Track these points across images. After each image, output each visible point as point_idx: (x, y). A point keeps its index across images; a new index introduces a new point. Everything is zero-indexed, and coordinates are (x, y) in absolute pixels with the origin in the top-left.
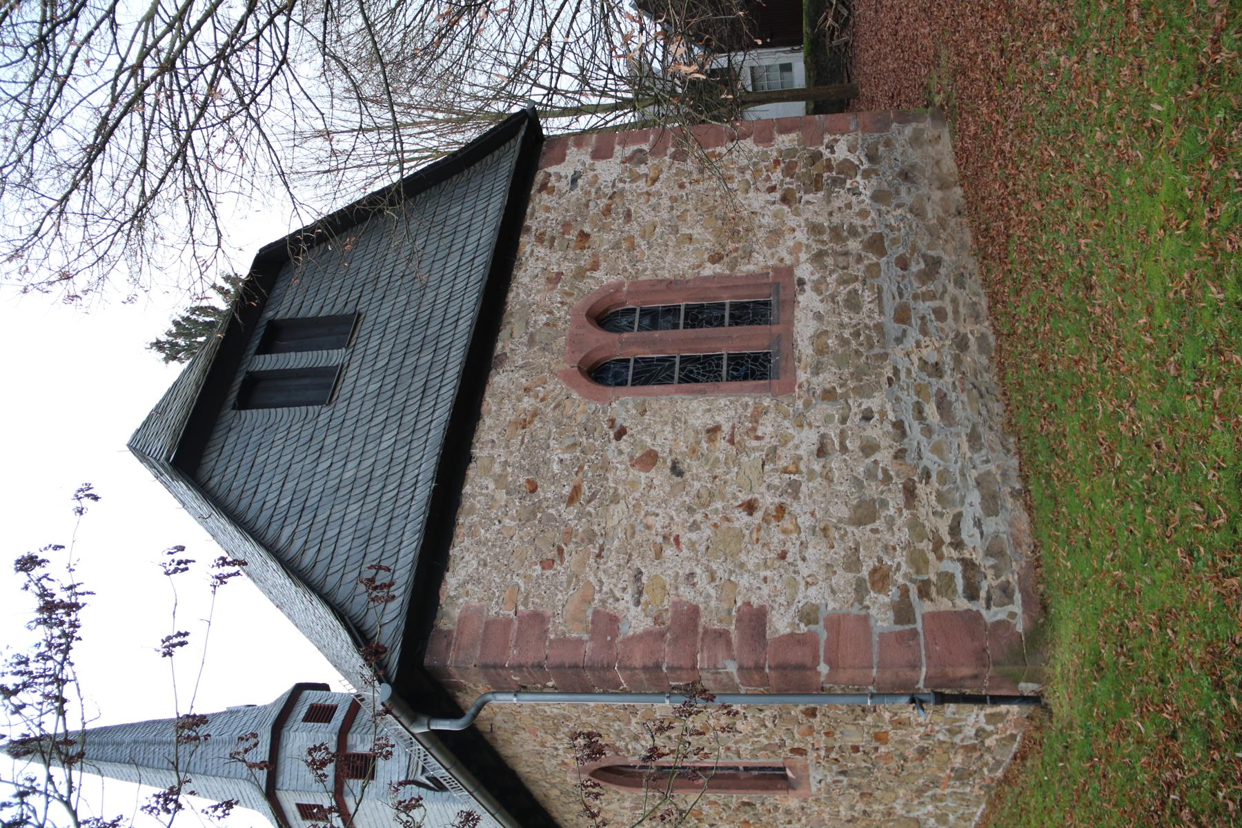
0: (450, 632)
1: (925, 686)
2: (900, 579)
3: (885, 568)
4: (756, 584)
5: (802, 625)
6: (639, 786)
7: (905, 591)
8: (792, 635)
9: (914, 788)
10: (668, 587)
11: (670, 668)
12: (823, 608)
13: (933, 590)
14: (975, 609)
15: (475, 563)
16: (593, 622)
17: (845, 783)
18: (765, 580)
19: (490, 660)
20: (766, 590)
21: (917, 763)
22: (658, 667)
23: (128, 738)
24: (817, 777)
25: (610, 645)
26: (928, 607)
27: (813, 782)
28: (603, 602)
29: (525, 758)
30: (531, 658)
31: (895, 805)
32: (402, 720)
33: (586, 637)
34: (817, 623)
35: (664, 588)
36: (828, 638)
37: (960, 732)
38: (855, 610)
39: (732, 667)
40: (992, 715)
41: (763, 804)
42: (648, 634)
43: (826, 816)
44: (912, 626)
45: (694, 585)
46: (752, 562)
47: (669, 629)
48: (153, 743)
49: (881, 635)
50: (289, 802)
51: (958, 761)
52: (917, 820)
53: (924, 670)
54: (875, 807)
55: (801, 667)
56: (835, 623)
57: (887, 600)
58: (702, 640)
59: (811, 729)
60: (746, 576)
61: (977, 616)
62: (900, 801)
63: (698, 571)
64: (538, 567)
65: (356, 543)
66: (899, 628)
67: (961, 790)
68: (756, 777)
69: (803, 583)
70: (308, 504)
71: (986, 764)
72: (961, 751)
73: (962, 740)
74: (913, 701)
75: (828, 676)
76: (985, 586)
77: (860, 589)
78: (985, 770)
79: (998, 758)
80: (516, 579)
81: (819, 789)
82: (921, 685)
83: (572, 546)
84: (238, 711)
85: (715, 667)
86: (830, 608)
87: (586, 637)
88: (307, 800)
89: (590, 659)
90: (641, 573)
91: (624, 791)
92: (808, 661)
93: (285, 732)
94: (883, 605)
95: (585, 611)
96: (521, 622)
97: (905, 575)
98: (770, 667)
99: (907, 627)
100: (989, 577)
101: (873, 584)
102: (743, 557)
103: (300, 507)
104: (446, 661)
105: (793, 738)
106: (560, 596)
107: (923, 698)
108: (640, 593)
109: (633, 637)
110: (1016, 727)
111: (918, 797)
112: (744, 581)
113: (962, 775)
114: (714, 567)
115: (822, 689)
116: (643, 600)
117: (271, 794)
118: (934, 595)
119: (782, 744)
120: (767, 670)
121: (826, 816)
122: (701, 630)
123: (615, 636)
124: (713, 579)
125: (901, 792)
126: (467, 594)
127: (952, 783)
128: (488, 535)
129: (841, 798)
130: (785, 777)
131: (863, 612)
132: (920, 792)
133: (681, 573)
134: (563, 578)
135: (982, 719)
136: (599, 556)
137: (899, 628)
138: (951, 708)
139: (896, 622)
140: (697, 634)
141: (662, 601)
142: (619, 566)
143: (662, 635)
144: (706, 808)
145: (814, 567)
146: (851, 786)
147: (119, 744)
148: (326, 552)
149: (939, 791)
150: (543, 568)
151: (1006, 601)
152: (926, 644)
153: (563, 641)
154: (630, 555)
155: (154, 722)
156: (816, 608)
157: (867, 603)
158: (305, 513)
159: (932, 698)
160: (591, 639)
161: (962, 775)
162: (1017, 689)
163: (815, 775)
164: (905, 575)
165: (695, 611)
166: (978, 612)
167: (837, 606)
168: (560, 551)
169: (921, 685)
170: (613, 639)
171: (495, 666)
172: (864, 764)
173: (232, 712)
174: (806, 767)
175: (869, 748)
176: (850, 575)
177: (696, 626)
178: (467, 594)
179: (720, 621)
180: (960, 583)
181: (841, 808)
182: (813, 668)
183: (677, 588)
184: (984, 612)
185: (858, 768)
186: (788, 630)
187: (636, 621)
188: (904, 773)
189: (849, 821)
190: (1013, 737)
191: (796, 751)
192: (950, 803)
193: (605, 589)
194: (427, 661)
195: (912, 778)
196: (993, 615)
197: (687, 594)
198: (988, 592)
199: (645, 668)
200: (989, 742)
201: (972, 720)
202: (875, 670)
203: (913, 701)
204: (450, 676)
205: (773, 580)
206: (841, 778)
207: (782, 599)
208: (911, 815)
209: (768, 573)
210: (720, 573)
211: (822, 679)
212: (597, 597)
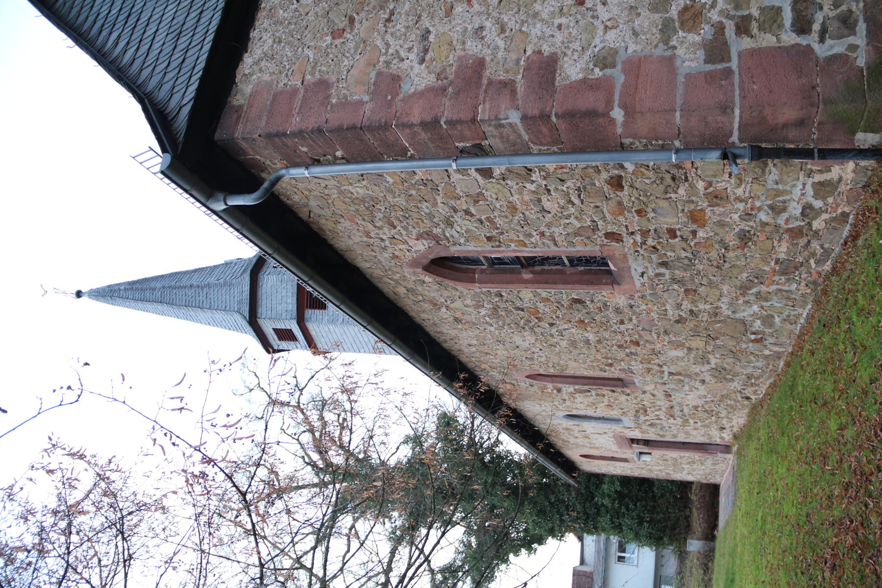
0: (240, 107)
1: (741, 140)
2: (714, 16)
3: (698, 6)
4: (548, 32)
5: (597, 70)
6: (472, 281)
7: (720, 29)
8: (584, 81)
9: (738, 284)
10: (455, 42)
11: (449, 122)
12: (622, 52)
13: (754, 25)
14: (804, 43)
15: (270, 41)
16: (374, 84)
17: (667, 277)
18: (560, 27)
19: (273, 130)
20: (559, 37)
21: (739, 252)
22: (436, 121)
23: (158, 285)
24: (638, 268)
25: (390, 104)
26: (746, 43)
27: (636, 275)
28: (388, 63)
29: (359, 252)
30: (311, 123)
31: (720, 304)
32: (194, 193)
33: (366, 98)
34: (614, 67)
35: (450, 44)
36: (626, 80)
37: (784, 210)
38: (660, 51)
39: (514, 117)
40: (821, 184)
41: (592, 301)
42: (430, 90)
43: (655, 316)
44: (725, 65)
45: (482, 38)
46: (546, 11)
47: (451, 83)
48: (174, 288)
49: (688, 76)
50: (268, 328)
51: (783, 250)
52: (743, 322)
53: (737, 112)
54: (702, 306)
55: (591, 114)
56: (635, 67)
57: (697, 38)
58: (486, 92)
59: (621, 208)
60: (539, 25)
61: (809, 49)
62: (725, 300)
63: (488, 24)
64: (329, 39)
65: (170, 37)
66: (709, 67)
67: (786, 288)
68: (581, 273)
69: (602, 27)
70: (134, 10)
71: (813, 254)
72: (786, 236)
73: (787, 221)
74: (725, 156)
75: (625, 124)
76: (819, 17)
77: (667, 30)
78: (812, 261)
79: (826, 246)
80: (306, 51)
81: (643, 284)
82: (735, 138)
83: (363, 14)
84: (231, 263)
85: (497, 118)
86: (630, 51)
87: (366, 98)
88: (280, 326)
89: (368, 119)
90: (429, 32)
91: (461, 287)
92: (601, 107)
93: (261, 276)
94: (693, 44)
95: (369, 73)
96: (306, 90)
97: (721, 12)
98: (556, 115)
99: (719, 66)
100: (825, 8)
101: (682, 24)
102: (538, 7)
103: (127, 14)
104: (234, 134)
105: (604, 218)
106: (346, 63)
107: (737, 151)
108: (426, 51)
109: (414, 94)
110: (849, 203)
111: (743, 295)
112: (537, 30)
113: (787, 269)
114: (506, 20)
115: (622, 145)
116: (428, 57)
117: (253, 322)
118: (755, 31)
119: (595, 229)
120: (554, 119)
121: (655, 316)
122: (485, 82)
123: (395, 95)
124: (503, 31)
125: (725, 288)
126: (261, 70)
127: (776, 278)
128: (286, 15)
129: (666, 295)
130: (610, 272)
131: (669, 53)
132: (744, 289)
133: (470, 27)
134: (351, 45)
135: (810, 190)
136: (389, 20)
137: (709, 67)
138: (773, 171)
139: (706, 62)
140: (481, 85)
141: (447, 57)
142: (408, 27)
143: (444, 89)
144: (541, 306)
145: (616, 11)
146: (674, 280)
147: (154, 289)
148: (144, 49)
149: (763, 288)
150: (334, 38)
151: (846, 32)
152: (742, 82)
153: (345, 104)
154: (420, 16)
155: (176, 273)
156: (615, 52)
157: (674, 42)
158: (130, 18)
159: (748, 152)
160: (372, 100)
161: (787, 269)
162: (853, 141)
163: (636, 267)
164: (721, 12)
165: (481, 63)
166: (809, 46)
167: (639, 48)
168: (352, 20)
169: (735, 138)
170: (393, 98)
171: (278, 135)
172: (684, 254)
173: (227, 264)
174: (625, 256)
175: (686, 233)
176: (656, 16)
177: (480, 78)
178: (261, 70)
179: (507, 72)
180: (788, 16)
181: (668, 307)
182: (606, 115)
183: (464, 43)
184: (816, 47)
185: (679, 259)
186: (581, 76)
187: (418, 77)
188: (727, 265)
189: (678, 322)
190: (845, 215)
191: (610, 235)
192: (776, 303)
193: (391, 51)
194: (217, 136)
195: (735, 271)
196: (822, 51)
197: (473, 47)
198: (823, 23)
199: (424, 125)
200: (817, 224)
201: (797, 192)
202: (678, 114)
203: (725, 156)
204: (245, 153)
205: (568, 27)
206: (662, 270)
207: (576, 45)
208: (737, 316)
209: (563, 20)
210: (511, 24)
211: (619, 130)
212: (382, 59)
